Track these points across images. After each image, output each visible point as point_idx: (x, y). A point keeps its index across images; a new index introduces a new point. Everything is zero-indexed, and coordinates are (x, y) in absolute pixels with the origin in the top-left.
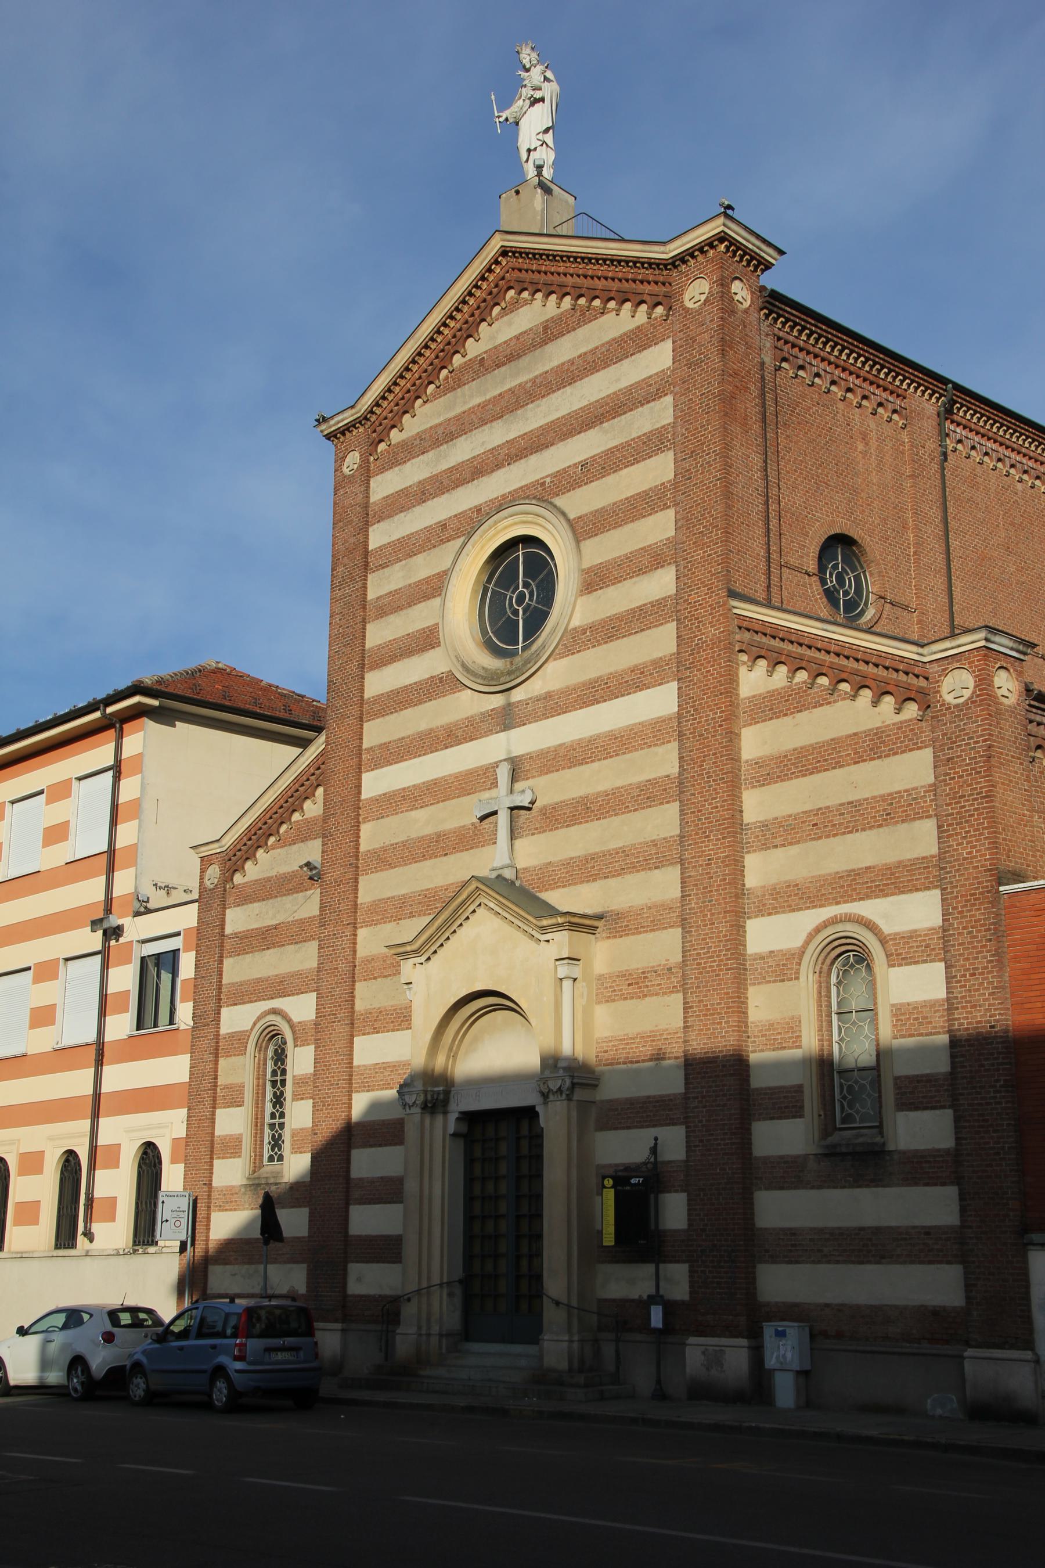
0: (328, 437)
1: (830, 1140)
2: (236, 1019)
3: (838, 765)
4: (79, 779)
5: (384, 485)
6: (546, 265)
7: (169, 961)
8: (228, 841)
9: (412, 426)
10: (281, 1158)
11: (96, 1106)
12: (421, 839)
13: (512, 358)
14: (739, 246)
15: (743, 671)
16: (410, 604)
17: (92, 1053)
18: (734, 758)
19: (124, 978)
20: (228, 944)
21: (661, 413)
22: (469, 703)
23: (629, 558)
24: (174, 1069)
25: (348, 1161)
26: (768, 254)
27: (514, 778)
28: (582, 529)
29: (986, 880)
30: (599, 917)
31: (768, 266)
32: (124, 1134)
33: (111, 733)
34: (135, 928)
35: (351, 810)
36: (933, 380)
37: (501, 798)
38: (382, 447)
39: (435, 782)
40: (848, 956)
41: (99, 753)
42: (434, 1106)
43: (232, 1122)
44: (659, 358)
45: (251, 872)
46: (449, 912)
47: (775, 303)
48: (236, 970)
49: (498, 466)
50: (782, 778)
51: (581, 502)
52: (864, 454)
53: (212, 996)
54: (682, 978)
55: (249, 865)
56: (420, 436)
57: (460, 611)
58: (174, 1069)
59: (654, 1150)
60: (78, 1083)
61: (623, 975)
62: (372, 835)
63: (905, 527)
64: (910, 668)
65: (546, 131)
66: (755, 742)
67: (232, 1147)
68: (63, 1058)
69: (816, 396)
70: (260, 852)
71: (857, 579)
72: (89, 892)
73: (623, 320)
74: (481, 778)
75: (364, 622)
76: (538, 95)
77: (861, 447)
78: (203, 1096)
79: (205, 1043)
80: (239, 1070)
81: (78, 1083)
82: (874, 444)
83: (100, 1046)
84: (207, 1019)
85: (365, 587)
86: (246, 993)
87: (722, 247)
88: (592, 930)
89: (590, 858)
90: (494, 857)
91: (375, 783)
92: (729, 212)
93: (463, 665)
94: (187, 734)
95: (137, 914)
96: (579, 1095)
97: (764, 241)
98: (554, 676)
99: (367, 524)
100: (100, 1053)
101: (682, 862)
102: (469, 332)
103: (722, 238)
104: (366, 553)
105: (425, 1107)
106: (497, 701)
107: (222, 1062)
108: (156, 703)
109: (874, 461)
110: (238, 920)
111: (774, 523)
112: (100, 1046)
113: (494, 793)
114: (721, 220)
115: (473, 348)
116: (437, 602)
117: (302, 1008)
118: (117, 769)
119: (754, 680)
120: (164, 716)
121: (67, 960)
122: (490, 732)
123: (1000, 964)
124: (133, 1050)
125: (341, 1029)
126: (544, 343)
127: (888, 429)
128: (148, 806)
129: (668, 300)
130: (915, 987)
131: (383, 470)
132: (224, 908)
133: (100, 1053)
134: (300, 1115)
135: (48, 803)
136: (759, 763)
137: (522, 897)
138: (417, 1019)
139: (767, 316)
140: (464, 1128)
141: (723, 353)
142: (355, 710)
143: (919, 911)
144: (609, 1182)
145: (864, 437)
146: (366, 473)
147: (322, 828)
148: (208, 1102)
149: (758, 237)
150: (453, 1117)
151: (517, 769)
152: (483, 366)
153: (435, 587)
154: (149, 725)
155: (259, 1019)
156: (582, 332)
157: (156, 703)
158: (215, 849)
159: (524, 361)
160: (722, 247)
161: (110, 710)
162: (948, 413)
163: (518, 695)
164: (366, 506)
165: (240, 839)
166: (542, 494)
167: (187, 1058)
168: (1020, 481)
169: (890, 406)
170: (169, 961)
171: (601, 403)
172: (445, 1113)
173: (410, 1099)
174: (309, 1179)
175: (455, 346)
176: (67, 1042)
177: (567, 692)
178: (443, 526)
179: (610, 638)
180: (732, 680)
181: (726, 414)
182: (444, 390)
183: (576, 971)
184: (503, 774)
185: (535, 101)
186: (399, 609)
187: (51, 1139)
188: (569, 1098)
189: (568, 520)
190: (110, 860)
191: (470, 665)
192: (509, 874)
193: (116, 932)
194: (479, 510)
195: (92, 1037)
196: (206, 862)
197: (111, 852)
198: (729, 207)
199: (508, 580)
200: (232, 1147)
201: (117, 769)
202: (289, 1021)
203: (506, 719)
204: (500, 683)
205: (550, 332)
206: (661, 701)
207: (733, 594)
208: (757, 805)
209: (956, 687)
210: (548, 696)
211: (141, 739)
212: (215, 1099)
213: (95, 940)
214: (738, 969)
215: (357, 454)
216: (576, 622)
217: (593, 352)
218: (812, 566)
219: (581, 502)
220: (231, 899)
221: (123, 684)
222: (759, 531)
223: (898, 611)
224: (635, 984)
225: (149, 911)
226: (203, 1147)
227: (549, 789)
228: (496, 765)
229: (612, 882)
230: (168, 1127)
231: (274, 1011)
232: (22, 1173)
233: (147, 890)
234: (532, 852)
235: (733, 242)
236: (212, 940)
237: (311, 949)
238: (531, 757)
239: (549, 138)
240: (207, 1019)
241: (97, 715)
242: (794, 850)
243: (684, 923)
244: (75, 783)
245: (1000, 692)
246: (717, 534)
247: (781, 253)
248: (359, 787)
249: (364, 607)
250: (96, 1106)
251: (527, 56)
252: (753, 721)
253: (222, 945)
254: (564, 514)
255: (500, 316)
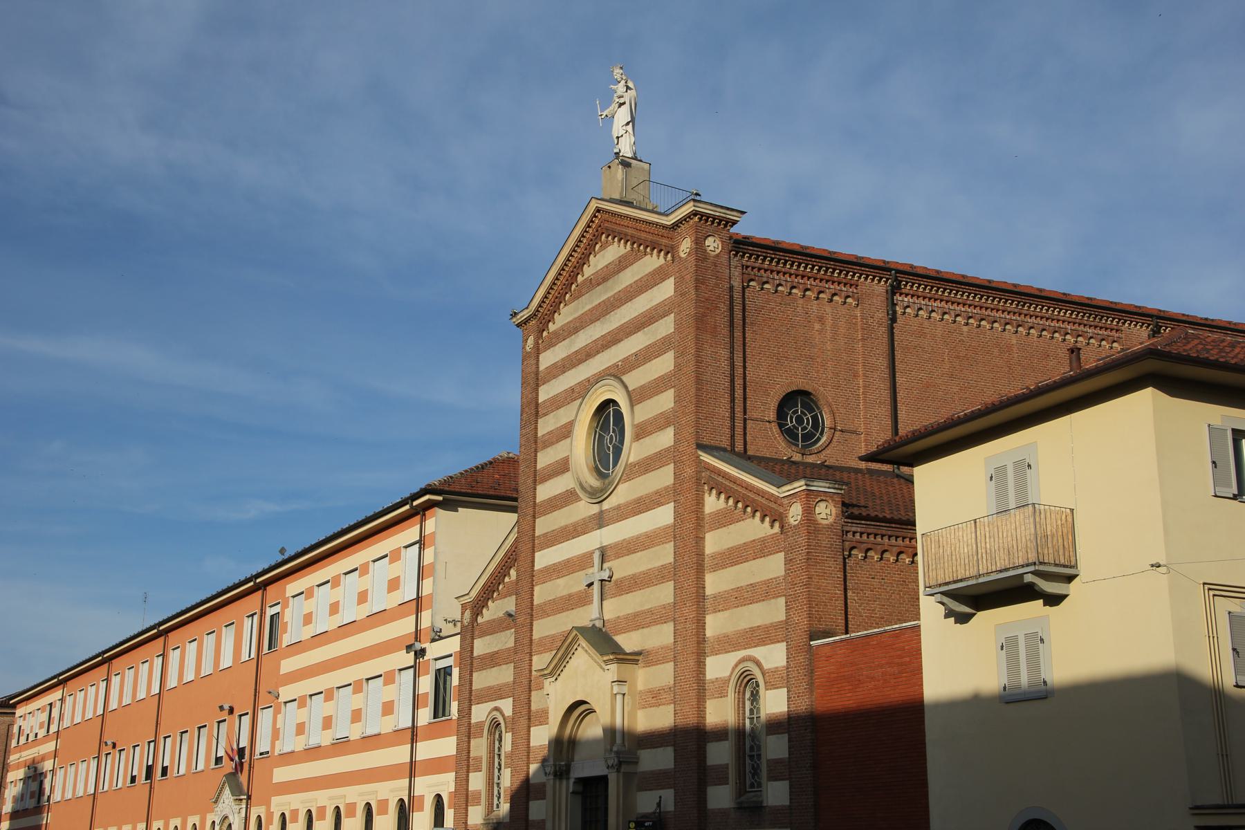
0: (519, 325)
1: (743, 799)
2: (480, 713)
3: (747, 561)
4: (406, 547)
5: (548, 359)
6: (618, 220)
7: (447, 671)
8: (474, 594)
9: (563, 317)
10: (760, 785)
11: (412, 769)
12: (561, 598)
13: (605, 280)
14: (708, 216)
15: (706, 495)
16: (558, 441)
17: (409, 733)
18: (700, 554)
19: (426, 684)
20: (708, 604)
21: (666, 326)
22: (584, 509)
23: (655, 418)
24: (446, 746)
25: (527, 809)
26: (732, 216)
27: (603, 560)
28: (635, 398)
29: (805, 637)
30: (639, 653)
31: (734, 223)
32: (427, 787)
33: (418, 518)
34: (434, 650)
35: (531, 577)
36: (879, 269)
37: (595, 573)
38: (545, 334)
39: (568, 561)
40: (747, 684)
41: (410, 533)
42: (561, 775)
43: (477, 782)
44: (667, 289)
45: (488, 615)
46: (564, 649)
47: (741, 245)
48: (482, 680)
49: (598, 352)
50: (724, 567)
51: (635, 379)
52: (820, 332)
53: (469, 698)
54: (674, 694)
55: (484, 611)
56: (562, 328)
57: (580, 447)
58: (446, 746)
59: (659, 805)
60: (400, 754)
61: (650, 691)
62: (541, 594)
63: (856, 376)
64: (776, 500)
65: (628, 124)
66: (714, 542)
67: (720, 776)
68: (395, 738)
69: (779, 300)
70: (490, 603)
71: (815, 419)
72: (406, 626)
73: (653, 262)
74: (583, 562)
75: (536, 451)
76: (622, 101)
77: (817, 326)
78: (463, 764)
79: (464, 729)
80: (479, 747)
81: (400, 754)
82: (829, 322)
83: (414, 728)
84: (465, 713)
85: (536, 428)
86: (728, 643)
87: (696, 219)
88: (636, 662)
89: (636, 615)
90: (587, 616)
91: (543, 559)
92: (698, 198)
93: (581, 485)
94: (465, 514)
95: (433, 640)
96: (624, 768)
97: (728, 209)
98: (623, 494)
99: (538, 386)
100: (413, 734)
101: (674, 620)
102: (584, 260)
103: (695, 213)
104: (537, 405)
105: (555, 775)
106: (595, 509)
107: (473, 742)
108: (440, 498)
109: (829, 335)
110: (482, 646)
111: (739, 393)
112: (414, 728)
113: (590, 571)
114: (692, 203)
115: (588, 271)
116: (568, 440)
117: (507, 706)
118: (421, 543)
119: (713, 503)
120: (449, 505)
121: (368, 680)
122: (593, 529)
123: (811, 691)
124: (434, 732)
125: (524, 722)
126: (619, 271)
127: (843, 310)
128: (440, 569)
129: (671, 250)
130: (775, 703)
131: (546, 349)
132: (473, 639)
133: (413, 734)
134: (507, 775)
135: (332, 588)
136: (713, 557)
137: (602, 640)
138: (551, 719)
139: (736, 255)
140: (580, 788)
141: (697, 288)
142: (530, 511)
143: (774, 656)
144: (632, 825)
145: (821, 320)
146: (537, 351)
147: (515, 590)
148: (465, 769)
149: (722, 207)
150: (572, 781)
151: (604, 555)
152: (593, 283)
153: (566, 432)
154: (440, 512)
155: (736, 666)
156: (635, 267)
157: (440, 498)
158: (467, 599)
159: (610, 282)
160: (696, 219)
161: (415, 503)
162: (895, 289)
163: (606, 505)
164: (537, 373)
165: (479, 593)
166: (616, 373)
167: (455, 738)
168: (967, 324)
169: (843, 294)
170: (447, 671)
171: (643, 315)
172: (568, 779)
173: (548, 770)
174: (507, 820)
175: (578, 268)
176: (369, 732)
177: (627, 504)
178: (572, 389)
179: (647, 471)
180: (700, 503)
181: (698, 329)
182: (576, 298)
183: (625, 689)
184: (596, 558)
185: (621, 105)
186: (552, 444)
187: (392, 791)
188: (618, 771)
189: (628, 391)
190: (418, 603)
191: (585, 485)
192: (599, 624)
193: (422, 652)
194: (588, 380)
195: (410, 724)
196: (464, 607)
197: (418, 599)
198: (697, 194)
199: (605, 427)
200: (720, 776)
201: (421, 543)
202: (503, 715)
203: (600, 521)
204: (598, 495)
205: (621, 265)
206: (664, 516)
207: (700, 447)
208: (715, 583)
209: (795, 513)
210: (618, 507)
211: (437, 521)
212: (468, 766)
213: (409, 659)
214: (701, 690)
215: (688, 240)
216: (631, 460)
217: (640, 280)
218: (772, 415)
219: (635, 379)
220: (476, 633)
221: (416, 490)
222: (725, 400)
223: (847, 435)
224: (654, 698)
225: (441, 638)
226: (464, 797)
227: (623, 568)
228: (592, 553)
229: (646, 631)
230: (445, 783)
231: (497, 709)
232: (347, 817)
233: (440, 624)
234: (615, 608)
235: (702, 215)
236: (468, 660)
237: (668, 629)
238: (611, 547)
239: (630, 128)
240: (465, 713)
241: (407, 507)
242: (727, 613)
243: (675, 660)
244: (403, 550)
245: (819, 517)
246: (692, 408)
247: (743, 213)
248: (533, 562)
249: (536, 442)
250: (412, 769)
251: (617, 73)
252: (711, 529)
253: (472, 664)
254: (626, 387)
255: (600, 250)
